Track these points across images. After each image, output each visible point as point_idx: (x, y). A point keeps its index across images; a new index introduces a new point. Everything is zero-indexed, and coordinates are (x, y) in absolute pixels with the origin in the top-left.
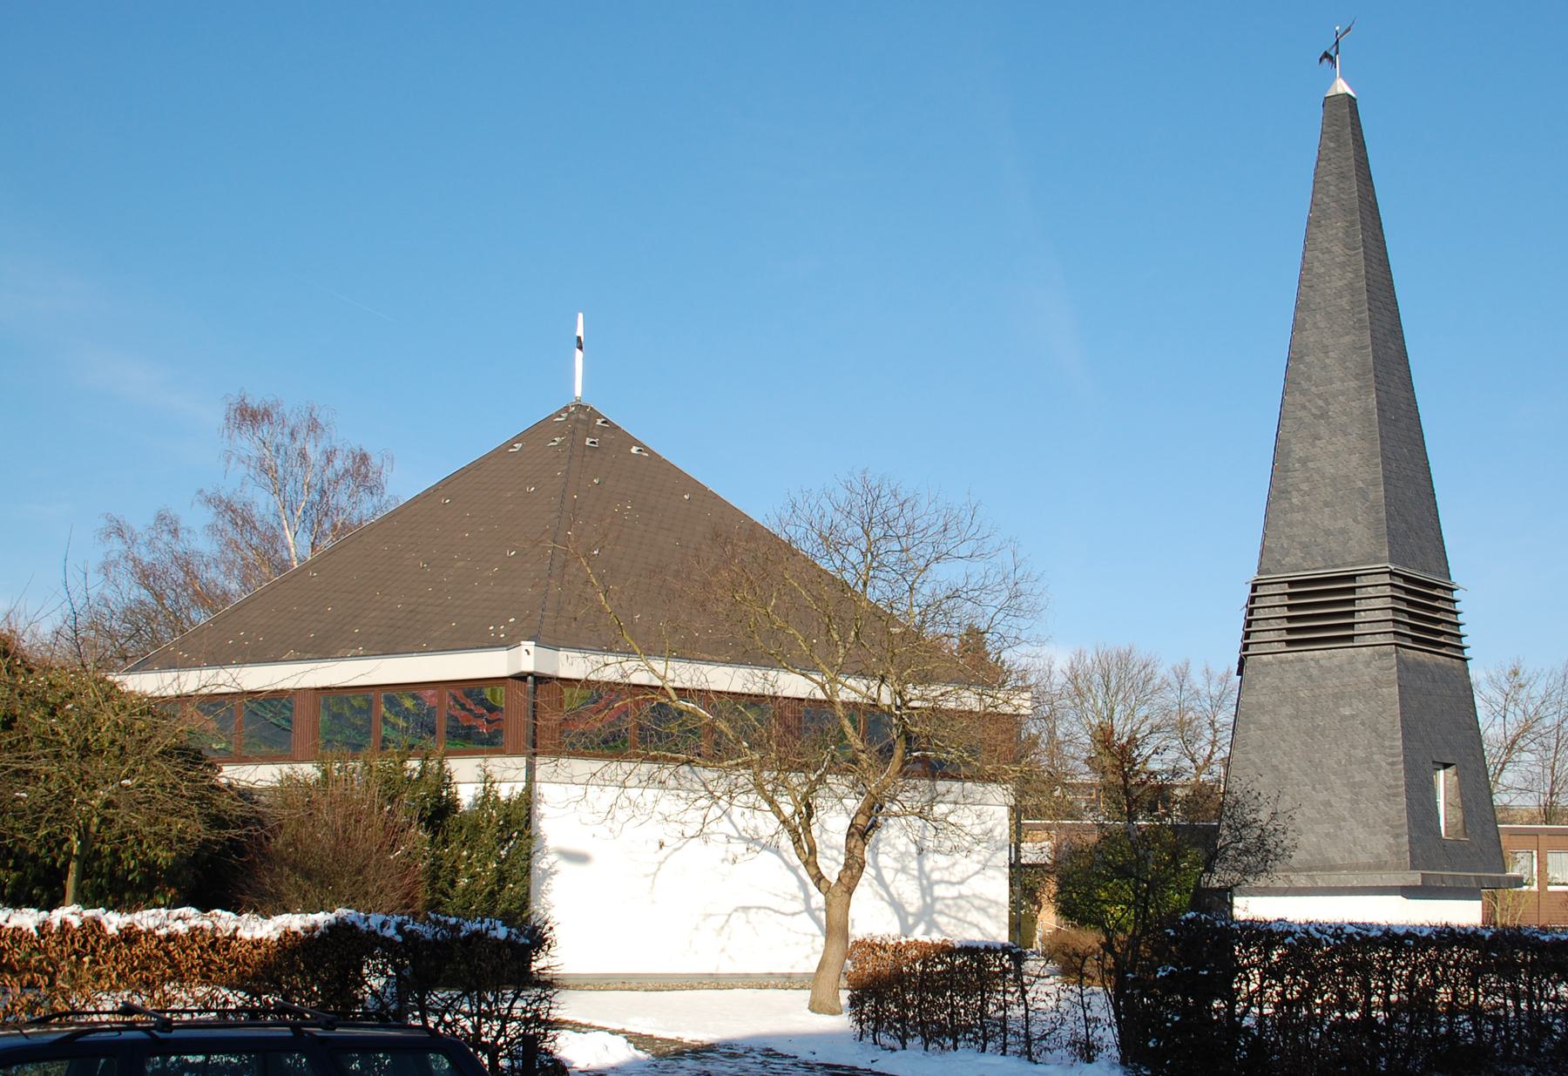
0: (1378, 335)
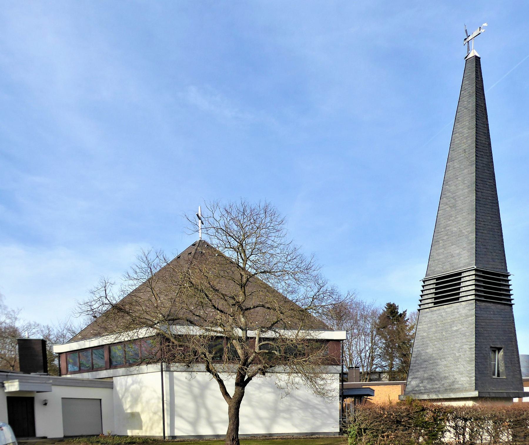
0: (480, 167)
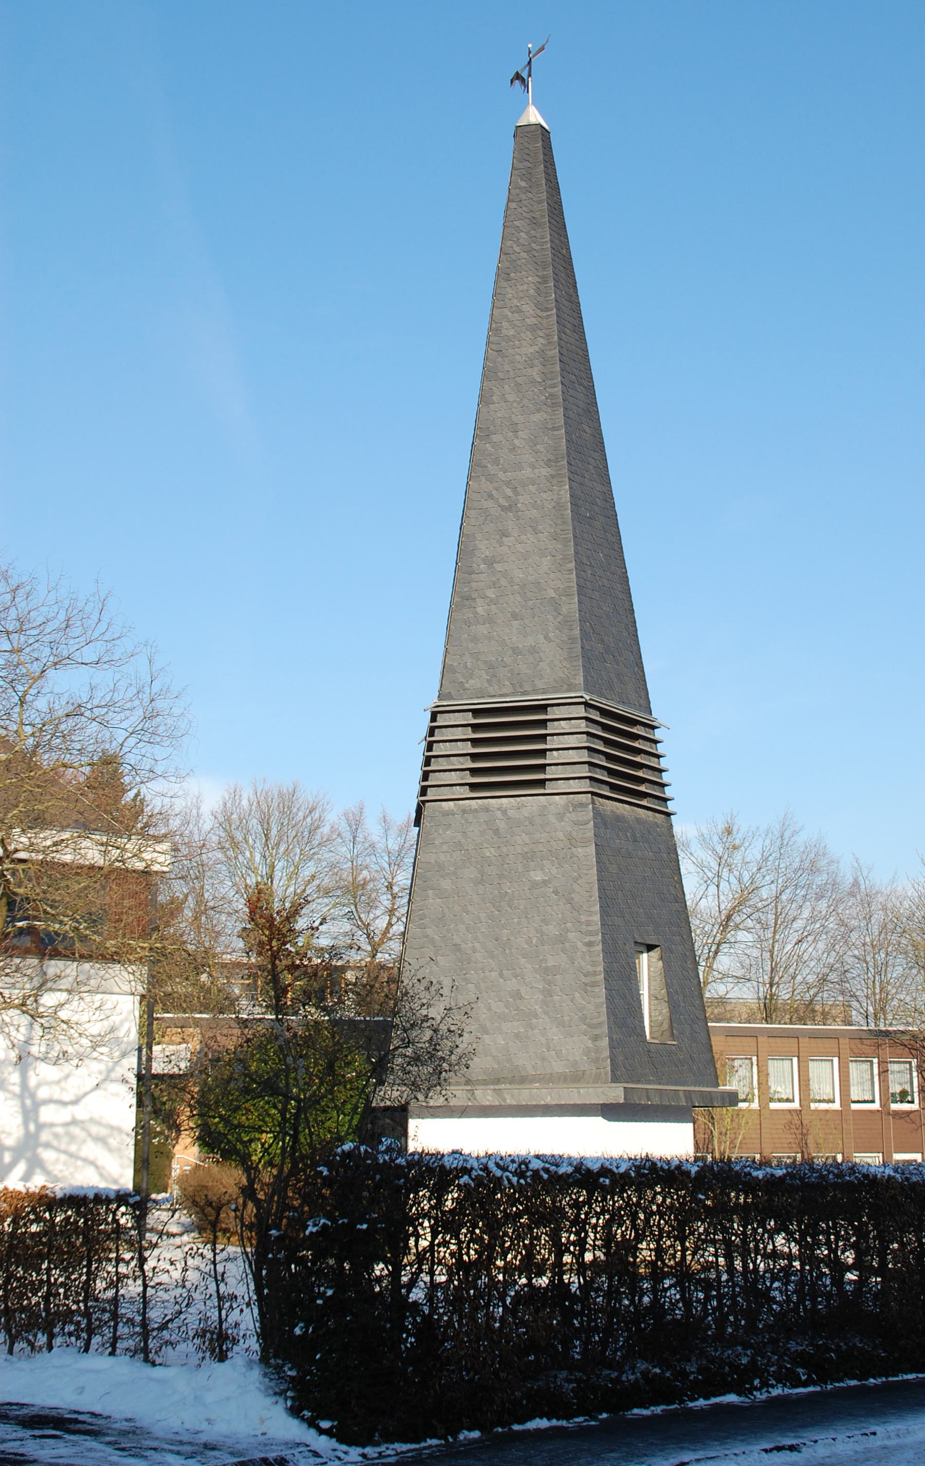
0: (572, 416)
